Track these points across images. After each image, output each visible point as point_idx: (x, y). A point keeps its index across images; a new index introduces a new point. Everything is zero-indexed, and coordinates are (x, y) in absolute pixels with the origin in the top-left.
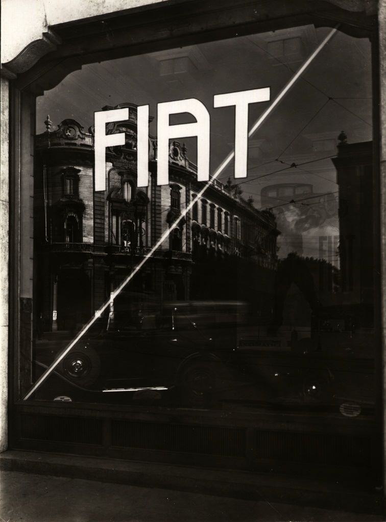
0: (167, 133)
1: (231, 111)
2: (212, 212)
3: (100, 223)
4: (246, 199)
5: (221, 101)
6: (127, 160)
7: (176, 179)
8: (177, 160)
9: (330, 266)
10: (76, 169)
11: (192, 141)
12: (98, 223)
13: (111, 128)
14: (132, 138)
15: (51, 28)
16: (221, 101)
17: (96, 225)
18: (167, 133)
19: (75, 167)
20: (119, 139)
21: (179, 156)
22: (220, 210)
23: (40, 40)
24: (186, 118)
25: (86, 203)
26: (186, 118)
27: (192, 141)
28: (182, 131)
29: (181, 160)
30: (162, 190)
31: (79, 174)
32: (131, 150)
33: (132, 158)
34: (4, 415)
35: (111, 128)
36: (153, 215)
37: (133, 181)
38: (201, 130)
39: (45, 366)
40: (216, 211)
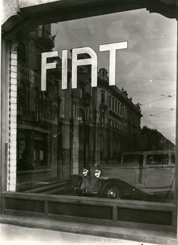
0: (76, 63)
1: (107, 53)
2: (116, 104)
3: (67, 108)
4: (129, 98)
5: (103, 48)
6: (81, 77)
7: (102, 87)
8: (104, 78)
9: (141, 128)
10: (57, 81)
11: (89, 67)
12: (66, 108)
13: (50, 60)
14: (59, 65)
15: (20, 9)
16: (103, 48)
17: (66, 109)
18: (76, 63)
19: (57, 80)
20: (53, 65)
21: (105, 75)
22: (119, 103)
23: (14, 16)
24: (87, 56)
25: (62, 98)
26: (87, 56)
27: (89, 67)
28: (83, 62)
29: (106, 78)
30: (97, 93)
31: (59, 84)
32: (82, 72)
33: (83, 76)
34: (105, 226)
35: (50, 60)
36: (93, 105)
37: (83, 88)
38: (93, 62)
39: (19, 172)
40: (117, 104)
